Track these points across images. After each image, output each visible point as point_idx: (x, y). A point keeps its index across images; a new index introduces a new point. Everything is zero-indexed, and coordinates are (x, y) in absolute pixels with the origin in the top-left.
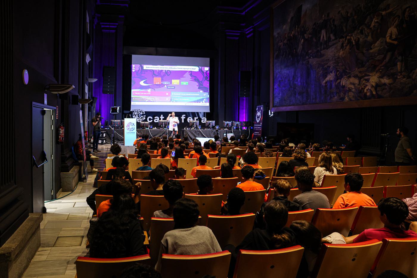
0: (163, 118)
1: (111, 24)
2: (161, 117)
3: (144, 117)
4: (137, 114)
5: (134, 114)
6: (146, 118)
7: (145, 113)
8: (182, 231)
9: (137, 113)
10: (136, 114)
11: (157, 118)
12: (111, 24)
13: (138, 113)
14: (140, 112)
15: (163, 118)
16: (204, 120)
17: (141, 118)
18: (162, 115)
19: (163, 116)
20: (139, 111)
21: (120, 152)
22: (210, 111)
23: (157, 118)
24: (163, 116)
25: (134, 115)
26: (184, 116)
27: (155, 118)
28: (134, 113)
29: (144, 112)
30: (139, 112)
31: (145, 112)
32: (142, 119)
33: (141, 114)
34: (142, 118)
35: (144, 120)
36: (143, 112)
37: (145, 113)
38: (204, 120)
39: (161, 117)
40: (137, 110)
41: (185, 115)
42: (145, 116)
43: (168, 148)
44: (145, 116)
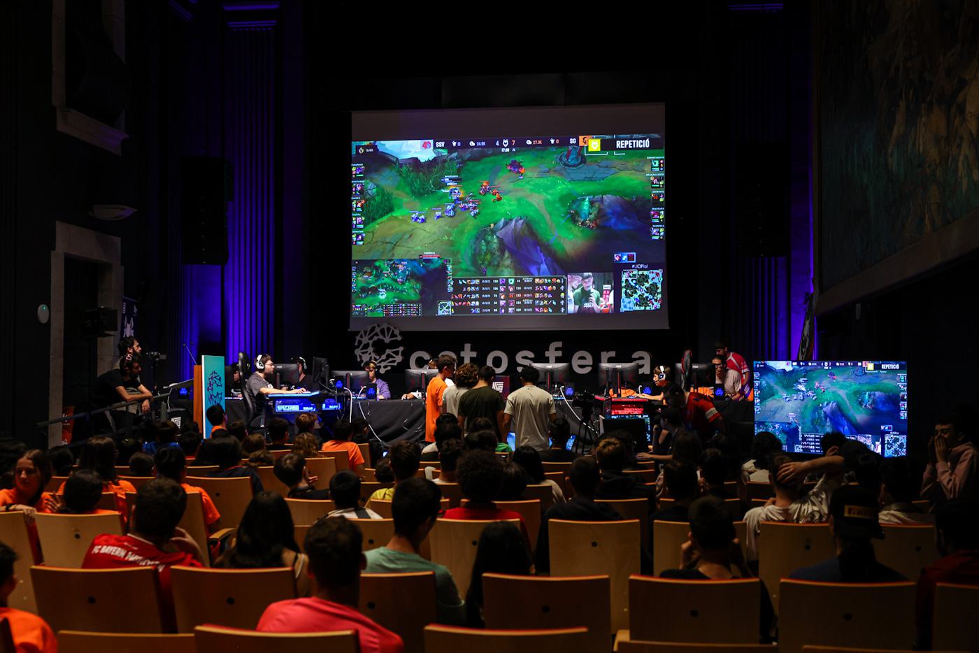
0: (474, 354)
1: (295, 408)
2: (462, 354)
3: (397, 353)
4: (371, 342)
5: (360, 342)
6: (407, 356)
7: (399, 338)
8: (290, 604)
9: (370, 339)
10: (365, 340)
11: (641, 358)
12: (295, 408)
13: (375, 338)
14: (382, 332)
15: (474, 354)
16: (582, 362)
17: (384, 357)
18: (468, 346)
19: (472, 350)
20: (378, 330)
21: (431, 159)
22: (670, 324)
23: (582, 366)
24: (472, 350)
25: (358, 347)
26: (557, 349)
27: (587, 370)
28: (358, 338)
29: (397, 332)
30: (377, 334)
31: (402, 333)
32: (391, 359)
33: (387, 340)
34: (389, 356)
35: (395, 364)
36: (393, 335)
37: (399, 338)
38: (582, 362)
39: (462, 354)
40: (369, 328)
41: (560, 344)
42: (401, 349)
43: (392, 472)
44: (401, 349)
